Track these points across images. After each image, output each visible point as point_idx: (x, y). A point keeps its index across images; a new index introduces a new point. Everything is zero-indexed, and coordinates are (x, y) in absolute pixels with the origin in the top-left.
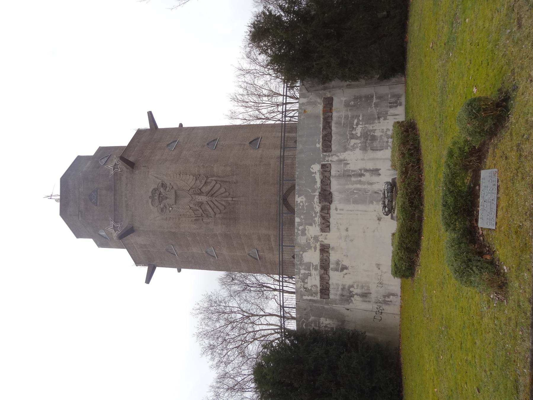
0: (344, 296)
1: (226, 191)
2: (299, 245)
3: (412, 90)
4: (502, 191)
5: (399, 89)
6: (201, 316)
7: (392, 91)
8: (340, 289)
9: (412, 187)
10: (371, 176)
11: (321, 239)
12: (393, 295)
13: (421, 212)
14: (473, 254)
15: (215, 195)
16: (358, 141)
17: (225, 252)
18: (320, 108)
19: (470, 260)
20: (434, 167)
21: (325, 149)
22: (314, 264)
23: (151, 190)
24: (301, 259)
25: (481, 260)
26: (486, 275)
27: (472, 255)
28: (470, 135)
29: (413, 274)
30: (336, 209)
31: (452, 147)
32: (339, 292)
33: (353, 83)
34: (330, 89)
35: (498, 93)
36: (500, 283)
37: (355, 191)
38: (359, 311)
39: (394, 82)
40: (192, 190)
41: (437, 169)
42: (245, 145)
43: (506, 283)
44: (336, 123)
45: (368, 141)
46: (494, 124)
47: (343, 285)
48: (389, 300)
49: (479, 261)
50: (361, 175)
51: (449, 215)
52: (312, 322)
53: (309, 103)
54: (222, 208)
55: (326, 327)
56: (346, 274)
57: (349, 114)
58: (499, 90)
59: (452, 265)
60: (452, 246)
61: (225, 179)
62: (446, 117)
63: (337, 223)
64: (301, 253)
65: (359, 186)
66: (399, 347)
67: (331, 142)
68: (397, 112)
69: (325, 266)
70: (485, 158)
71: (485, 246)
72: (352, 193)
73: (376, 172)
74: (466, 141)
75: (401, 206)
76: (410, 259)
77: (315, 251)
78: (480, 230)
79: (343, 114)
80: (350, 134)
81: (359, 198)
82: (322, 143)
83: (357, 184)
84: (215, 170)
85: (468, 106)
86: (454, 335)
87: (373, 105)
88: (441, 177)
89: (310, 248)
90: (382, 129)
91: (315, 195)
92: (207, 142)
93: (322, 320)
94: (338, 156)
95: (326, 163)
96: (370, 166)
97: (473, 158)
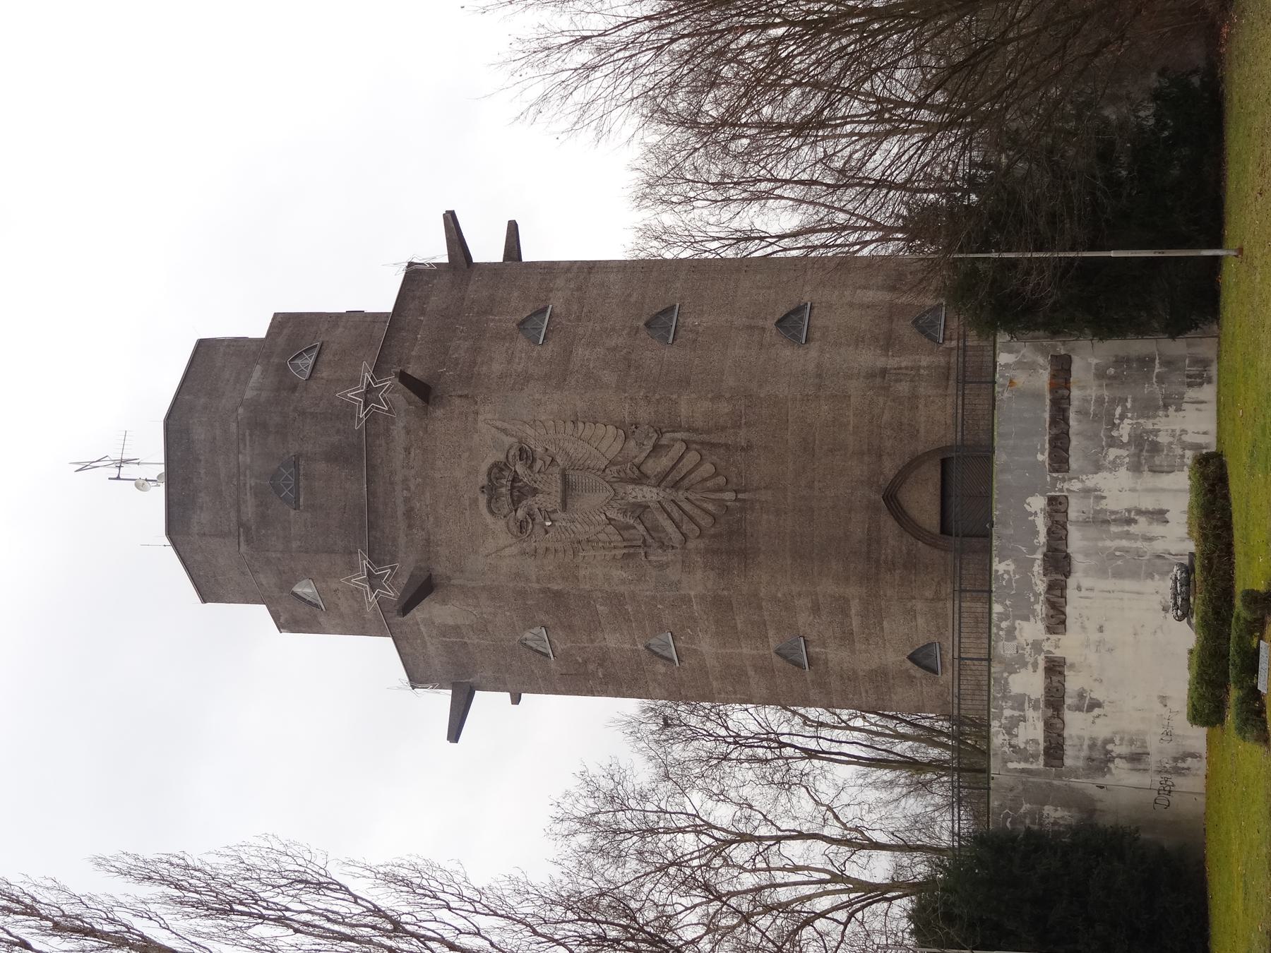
1: (716, 474)
2: (1002, 661)
5: (1206, 348)
6: (584, 839)
8: (1085, 747)
10: (1150, 523)
12: (1193, 756)
15: (686, 483)
16: (1124, 452)
17: (707, 646)
18: (1043, 379)
23: (484, 468)
24: (1005, 688)
30: (1079, 588)
32: (1085, 752)
37: (1118, 553)
38: (1125, 788)
40: (614, 468)
42: (763, 329)
45: (1144, 453)
47: (1091, 739)
48: (1185, 765)
50: (1129, 521)
52: (1025, 815)
54: (705, 521)
55: (1055, 823)
56: (1098, 716)
57: (1106, 393)
61: (714, 438)
64: (1005, 675)
67: (1067, 451)
68: (1202, 398)
69: (1054, 701)
72: (1112, 556)
73: (1159, 515)
79: (1093, 392)
83: (1121, 539)
84: (684, 410)
89: (1025, 665)
92: (645, 318)
93: (1048, 810)
94: (1083, 481)
96: (1148, 503)
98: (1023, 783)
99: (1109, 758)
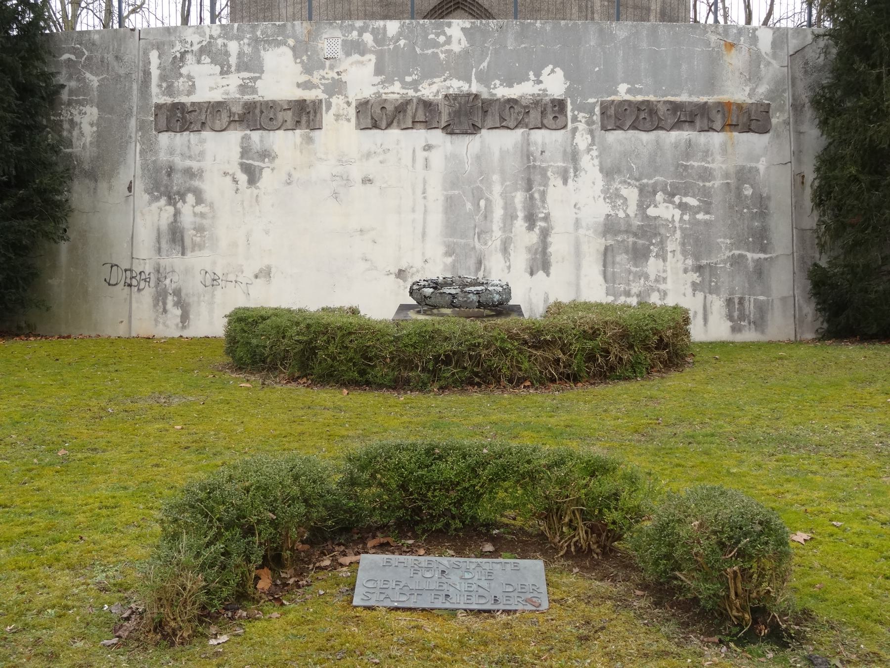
0: (169, 175)
2: (313, 36)
3: (781, 358)
4: (477, 624)
5: (779, 327)
7: (777, 304)
8: (188, 163)
9: (495, 360)
10: (528, 249)
11: (337, 101)
13: (422, 387)
14: (272, 540)
16: (632, 209)
18: (737, 92)
19: (249, 531)
20: (552, 420)
21: (612, 111)
22: (259, 83)
24: (272, 42)
25: (252, 567)
26: (194, 582)
27: (265, 536)
28: (662, 528)
29: (240, 369)
30: (428, 148)
31: (619, 473)
32: (180, 163)
33: (808, 192)
34: (796, 122)
35: (798, 609)
36: (173, 624)
37: (482, 203)
38: (125, 219)
39: (800, 308)
41: (549, 429)
43: (172, 644)
44: (689, 143)
45: (631, 240)
46: (696, 600)
47: (201, 172)
49: (248, 560)
50: (531, 220)
51: (399, 466)
53: (756, 59)
56: (235, 181)
57: (717, 183)
58: (806, 615)
59: (231, 478)
60: (296, 478)
62: (706, 453)
63: (386, 151)
64: (291, 42)
65: (498, 212)
66: (36, 336)
67: (634, 127)
68: (712, 319)
69: (255, 115)
70: (582, 568)
71: (300, 574)
72: (478, 195)
73: (541, 261)
74: (638, 514)
75: (438, 331)
76: (284, 358)
77: (299, 85)
78: (353, 558)
79: (718, 164)
80: (655, 184)
81: (463, 212)
82: (629, 103)
83: (505, 208)
85: (761, 523)
86: (37, 484)
87: (737, 252)
88: (527, 441)
89: (308, 70)
90: (665, 279)
91: (469, 81)
93: (92, 112)
94: (589, 150)
95: (569, 114)
96: (558, 246)
97: (582, 534)
98: (128, 75)
99: (173, 198)
